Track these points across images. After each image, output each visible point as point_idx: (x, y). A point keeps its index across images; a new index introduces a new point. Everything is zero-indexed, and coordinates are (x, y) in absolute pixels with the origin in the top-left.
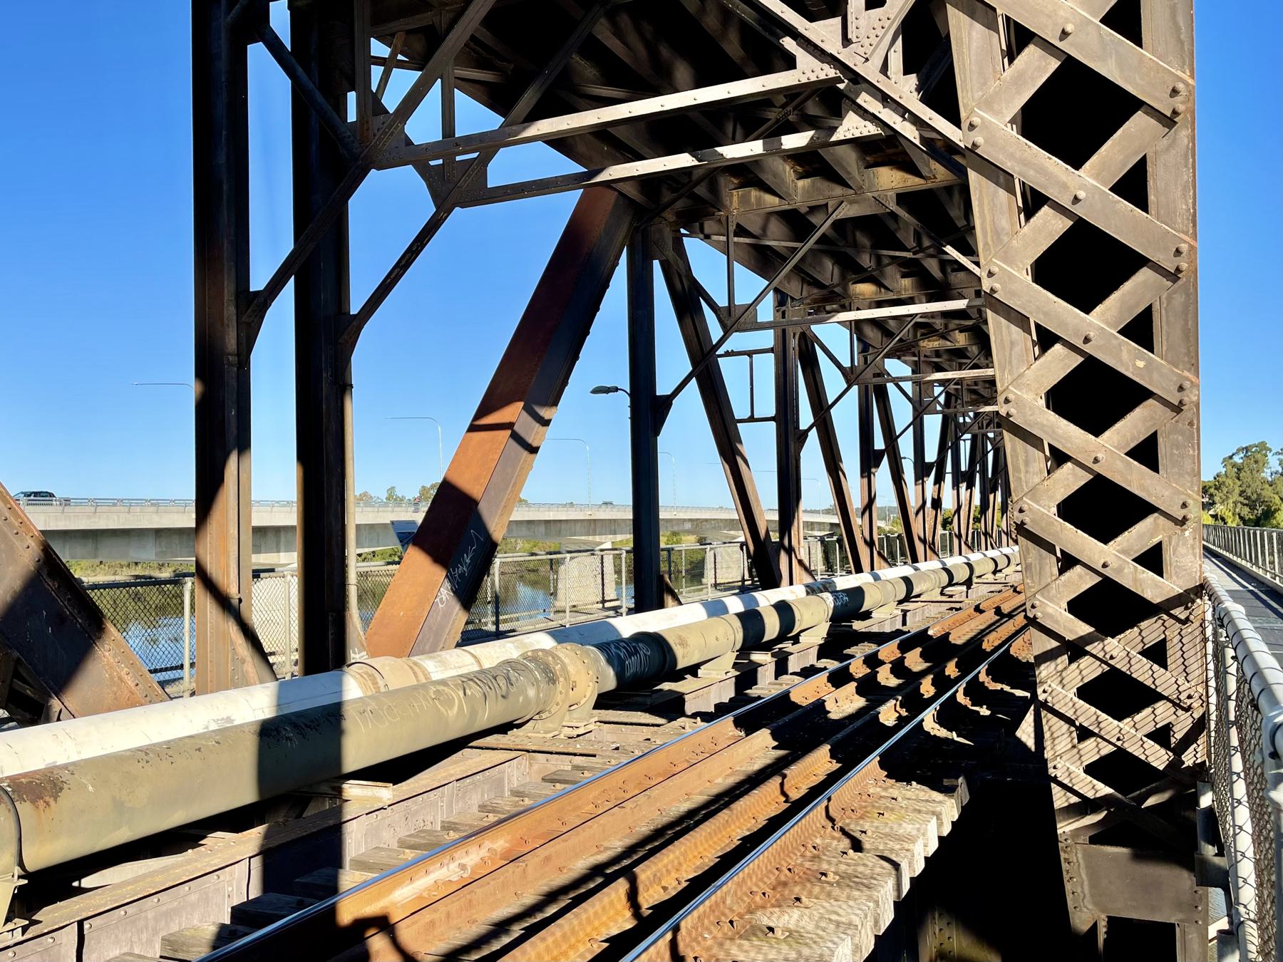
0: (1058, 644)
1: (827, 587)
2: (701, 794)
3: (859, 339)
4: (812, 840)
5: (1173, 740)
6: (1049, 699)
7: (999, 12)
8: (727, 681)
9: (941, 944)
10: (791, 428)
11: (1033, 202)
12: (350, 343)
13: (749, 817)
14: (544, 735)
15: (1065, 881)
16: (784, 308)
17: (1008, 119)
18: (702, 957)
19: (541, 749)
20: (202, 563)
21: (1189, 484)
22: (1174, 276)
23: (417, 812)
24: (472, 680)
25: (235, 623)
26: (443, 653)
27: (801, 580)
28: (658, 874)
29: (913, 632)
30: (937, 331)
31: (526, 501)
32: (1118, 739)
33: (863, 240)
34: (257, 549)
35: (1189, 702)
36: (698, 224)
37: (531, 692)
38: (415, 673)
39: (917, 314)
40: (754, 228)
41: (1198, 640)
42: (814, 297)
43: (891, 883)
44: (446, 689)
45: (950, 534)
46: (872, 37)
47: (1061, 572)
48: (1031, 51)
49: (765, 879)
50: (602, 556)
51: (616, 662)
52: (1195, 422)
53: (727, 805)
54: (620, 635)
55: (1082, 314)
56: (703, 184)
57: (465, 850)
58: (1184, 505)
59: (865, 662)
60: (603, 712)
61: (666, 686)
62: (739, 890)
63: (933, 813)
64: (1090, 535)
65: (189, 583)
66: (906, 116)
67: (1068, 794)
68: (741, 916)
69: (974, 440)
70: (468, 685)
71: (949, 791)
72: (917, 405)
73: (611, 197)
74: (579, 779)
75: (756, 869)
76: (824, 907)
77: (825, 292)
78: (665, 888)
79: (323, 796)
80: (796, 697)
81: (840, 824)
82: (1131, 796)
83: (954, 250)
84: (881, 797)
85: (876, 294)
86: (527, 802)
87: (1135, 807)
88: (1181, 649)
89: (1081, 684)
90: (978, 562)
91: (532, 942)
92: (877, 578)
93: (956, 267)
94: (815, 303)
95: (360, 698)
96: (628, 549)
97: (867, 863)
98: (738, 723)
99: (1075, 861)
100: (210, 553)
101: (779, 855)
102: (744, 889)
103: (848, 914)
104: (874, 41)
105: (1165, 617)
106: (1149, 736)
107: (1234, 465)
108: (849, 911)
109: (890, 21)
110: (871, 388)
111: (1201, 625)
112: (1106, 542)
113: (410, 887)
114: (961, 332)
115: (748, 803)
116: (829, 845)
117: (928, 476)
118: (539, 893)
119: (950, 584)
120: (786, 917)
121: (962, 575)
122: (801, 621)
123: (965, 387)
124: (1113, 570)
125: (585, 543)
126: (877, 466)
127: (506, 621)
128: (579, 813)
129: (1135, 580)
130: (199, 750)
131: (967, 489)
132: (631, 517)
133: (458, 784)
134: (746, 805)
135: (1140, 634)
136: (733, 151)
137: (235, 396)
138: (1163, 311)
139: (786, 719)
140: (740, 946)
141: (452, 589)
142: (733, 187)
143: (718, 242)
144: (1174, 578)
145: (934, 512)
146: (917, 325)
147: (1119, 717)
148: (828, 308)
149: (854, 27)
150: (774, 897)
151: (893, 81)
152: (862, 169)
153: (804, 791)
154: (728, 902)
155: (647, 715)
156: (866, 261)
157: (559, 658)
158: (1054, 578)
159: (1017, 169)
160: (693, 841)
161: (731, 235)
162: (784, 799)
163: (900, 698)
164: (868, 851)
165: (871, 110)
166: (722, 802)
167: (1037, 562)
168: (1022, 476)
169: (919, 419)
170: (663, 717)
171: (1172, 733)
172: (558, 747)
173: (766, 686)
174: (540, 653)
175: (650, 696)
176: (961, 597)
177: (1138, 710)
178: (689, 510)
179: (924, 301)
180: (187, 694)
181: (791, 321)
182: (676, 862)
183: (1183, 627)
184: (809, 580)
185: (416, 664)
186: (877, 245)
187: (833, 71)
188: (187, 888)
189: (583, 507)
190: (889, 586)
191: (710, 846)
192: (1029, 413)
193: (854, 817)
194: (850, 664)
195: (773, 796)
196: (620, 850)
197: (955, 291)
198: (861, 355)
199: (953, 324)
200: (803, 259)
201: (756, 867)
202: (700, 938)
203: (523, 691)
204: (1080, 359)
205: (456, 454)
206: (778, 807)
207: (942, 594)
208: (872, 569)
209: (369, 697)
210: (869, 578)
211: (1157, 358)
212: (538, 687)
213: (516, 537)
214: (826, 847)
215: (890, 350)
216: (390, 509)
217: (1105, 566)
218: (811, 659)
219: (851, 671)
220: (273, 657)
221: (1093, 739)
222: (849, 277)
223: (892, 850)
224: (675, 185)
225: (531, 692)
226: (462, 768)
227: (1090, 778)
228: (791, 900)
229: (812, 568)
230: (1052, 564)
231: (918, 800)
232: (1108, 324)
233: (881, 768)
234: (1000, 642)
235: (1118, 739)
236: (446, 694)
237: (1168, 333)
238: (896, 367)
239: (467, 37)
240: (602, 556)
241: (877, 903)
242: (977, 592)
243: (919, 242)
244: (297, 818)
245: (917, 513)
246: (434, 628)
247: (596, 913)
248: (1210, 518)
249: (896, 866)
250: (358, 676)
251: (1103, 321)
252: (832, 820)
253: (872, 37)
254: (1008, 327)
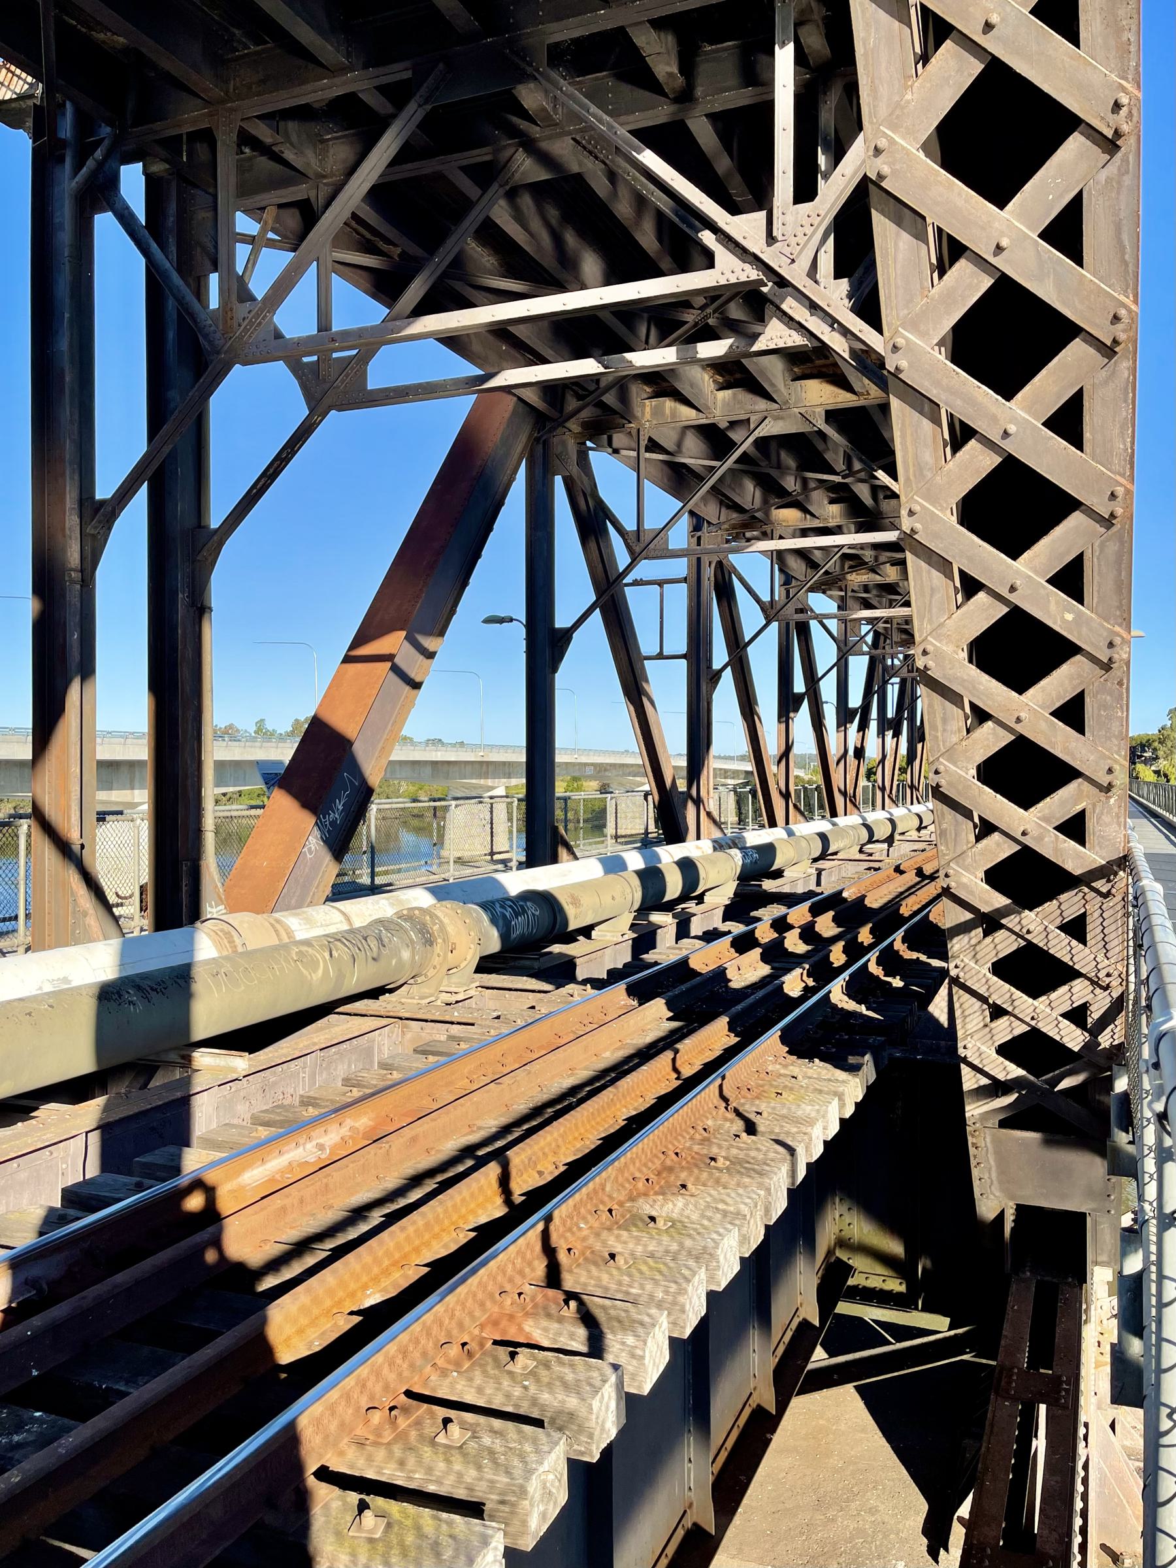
0: (972, 916)
1: (736, 843)
2: (586, 1069)
3: (781, 570)
4: (703, 1122)
5: (1090, 1020)
6: (961, 975)
7: (929, 220)
8: (624, 944)
9: (841, 1231)
10: (703, 666)
11: (961, 435)
12: (210, 561)
13: (637, 1096)
14: (419, 1001)
15: (972, 1166)
16: (699, 534)
17: (935, 342)
18: (576, 1248)
19: (415, 1017)
20: (39, 802)
21: (1116, 749)
22: (1107, 522)
23: (275, 1083)
24: (339, 940)
25: (77, 871)
26: (309, 910)
27: (709, 833)
28: (534, 1158)
29: (826, 893)
30: (867, 563)
31: (411, 739)
32: (1033, 1018)
33: (790, 461)
34: (106, 784)
35: (1107, 980)
36: (605, 436)
37: (406, 955)
38: (276, 931)
39: (843, 546)
40: (668, 443)
41: (1120, 914)
42: (733, 522)
43: (785, 1169)
44: (310, 950)
45: (873, 786)
46: (800, 235)
47: (978, 839)
48: (962, 265)
49: (650, 1164)
50: (492, 804)
51: (501, 922)
52: (1125, 681)
53: (613, 1081)
54: (507, 892)
55: (1009, 560)
56: (613, 392)
57: (323, 1129)
58: (1110, 771)
59: (772, 926)
60: (485, 976)
61: (556, 948)
62: (620, 1176)
63: (835, 1094)
64: (1010, 800)
65: (24, 826)
66: (836, 326)
67: (978, 1075)
68: (621, 1204)
69: (903, 683)
70: (335, 946)
71: (854, 1069)
72: (842, 645)
73: (510, 402)
74: (453, 1051)
75: (640, 1153)
76: (711, 1195)
77: (745, 517)
78: (540, 1173)
79: (171, 1064)
80: (695, 964)
81: (734, 1105)
82: (1044, 1078)
83: (886, 476)
84: (781, 1075)
85: (801, 520)
86: (396, 1076)
87: (1048, 1092)
88: (1101, 924)
89: (995, 959)
90: (902, 818)
91: (392, 1232)
92: (790, 833)
93: (889, 493)
94: (733, 529)
95: (214, 959)
96: (521, 796)
97: (761, 1146)
98: (631, 991)
99: (983, 1145)
100: (49, 793)
101: (666, 1138)
102: (626, 1175)
103: (736, 1203)
104: (802, 240)
105: (1086, 890)
106: (1065, 1015)
108: (738, 1199)
109: (819, 218)
110: (792, 625)
111: (1123, 899)
112: (1026, 806)
113: (261, 1169)
114: (892, 565)
115: (636, 1080)
116: (720, 1127)
117: (852, 722)
118: (403, 1176)
119: (871, 841)
120: (670, 1205)
121: (882, 832)
122: (706, 879)
123: (895, 626)
124: (1033, 838)
125: (475, 787)
126: (796, 710)
127: (380, 874)
128: (451, 1088)
129: (1056, 850)
130: (30, 1014)
131: (893, 737)
132: (524, 759)
133: (323, 1053)
134: (633, 1082)
135: (1059, 907)
136: (644, 359)
137: (78, 617)
138: (1095, 560)
139: (683, 988)
140: (618, 1237)
141: (322, 837)
142: (646, 396)
143: (629, 457)
144: (1097, 848)
145: (857, 762)
146: (845, 557)
147: (1035, 997)
148: (748, 535)
149: (780, 224)
150: (658, 1183)
151: (822, 285)
152: (788, 378)
153: (697, 1067)
154: (608, 1189)
155: (534, 981)
156: (790, 483)
157: (438, 917)
158: (970, 845)
159: (943, 397)
160: (574, 1122)
161: (642, 450)
162: (676, 1076)
163: (807, 966)
164: (763, 1134)
165: (797, 318)
166: (608, 1078)
167: (953, 828)
168: (939, 734)
169: (843, 660)
170: (551, 983)
171: (1089, 1013)
172: (434, 1014)
173: (666, 951)
174: (417, 912)
175: (538, 959)
176: (881, 855)
177: (1054, 988)
178: (592, 753)
179: (853, 529)
180: (22, 949)
181: (706, 549)
182: (554, 1145)
183: (1105, 901)
184: (717, 834)
185: (278, 921)
186: (804, 466)
187: (756, 272)
188: (15, 1165)
189: (474, 747)
190: (804, 843)
191: (592, 1127)
192: (949, 667)
193: (749, 1096)
194: (756, 928)
195: (663, 1073)
196: (494, 1130)
197: (887, 521)
198: (783, 588)
199: (885, 556)
200: (721, 480)
201: (640, 1151)
202: (575, 1229)
203: (396, 953)
204: (1006, 610)
205: (329, 688)
206: (669, 1084)
207: (861, 851)
208: (787, 823)
209: (226, 958)
210: (783, 834)
211: (1088, 612)
212: (414, 948)
213: (400, 779)
214: (717, 1129)
215: (814, 583)
216: (258, 744)
217: (1024, 834)
218: (717, 922)
219: (757, 936)
220: (120, 908)
221: (1006, 1018)
222: (772, 502)
223: (788, 1133)
224: (581, 392)
225: (406, 955)
226: (326, 1036)
227: (1002, 1059)
228: (676, 1186)
229: (723, 820)
230: (968, 831)
231: (819, 1079)
232: (1036, 572)
233: (783, 1044)
234: (919, 906)
235: (1033, 1018)
236: (311, 956)
237: (1099, 584)
238: (822, 603)
239: (346, 215)
240: (492, 804)
241: (768, 1190)
242: (899, 850)
243: (849, 465)
244: (140, 1089)
245: (838, 763)
246: (301, 881)
247: (463, 1200)
248: (1152, 774)
249: (792, 1151)
250: (212, 933)
251: (1031, 569)
252: (725, 1100)
253: (800, 235)
254: (929, 572)
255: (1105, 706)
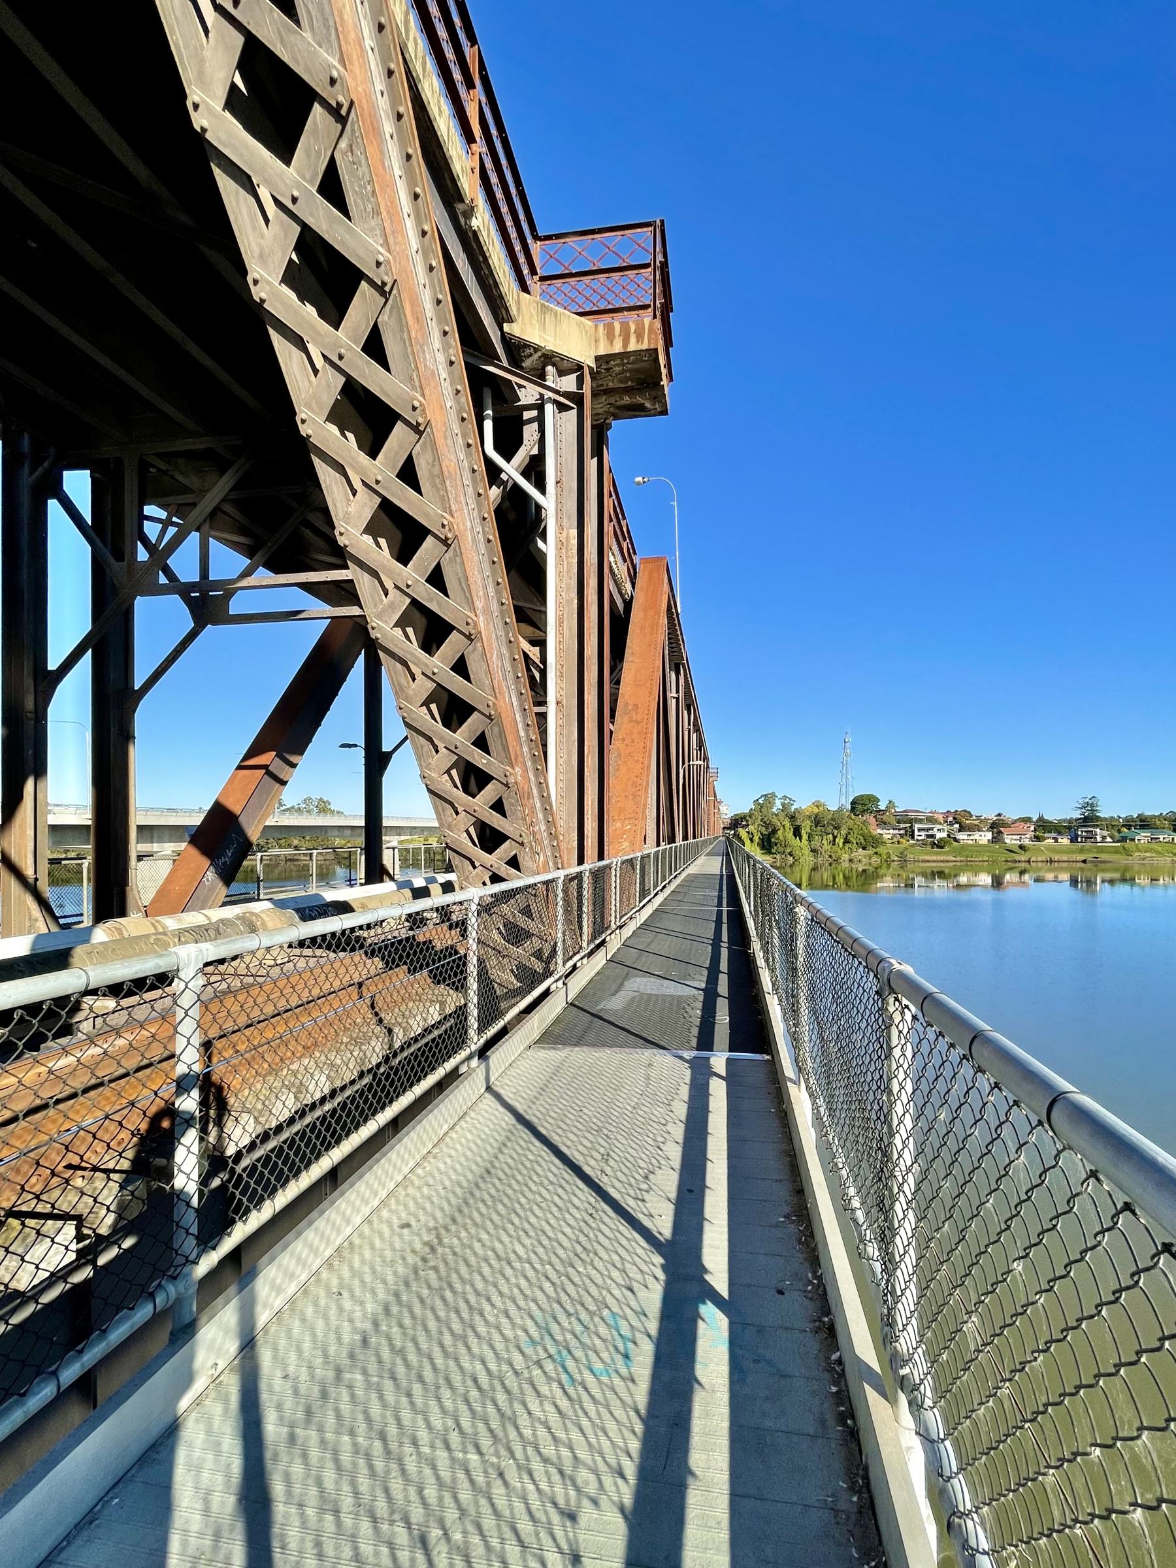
44: (164, 937)
107: (759, 804)
185: (157, 921)
255: (511, 804)
